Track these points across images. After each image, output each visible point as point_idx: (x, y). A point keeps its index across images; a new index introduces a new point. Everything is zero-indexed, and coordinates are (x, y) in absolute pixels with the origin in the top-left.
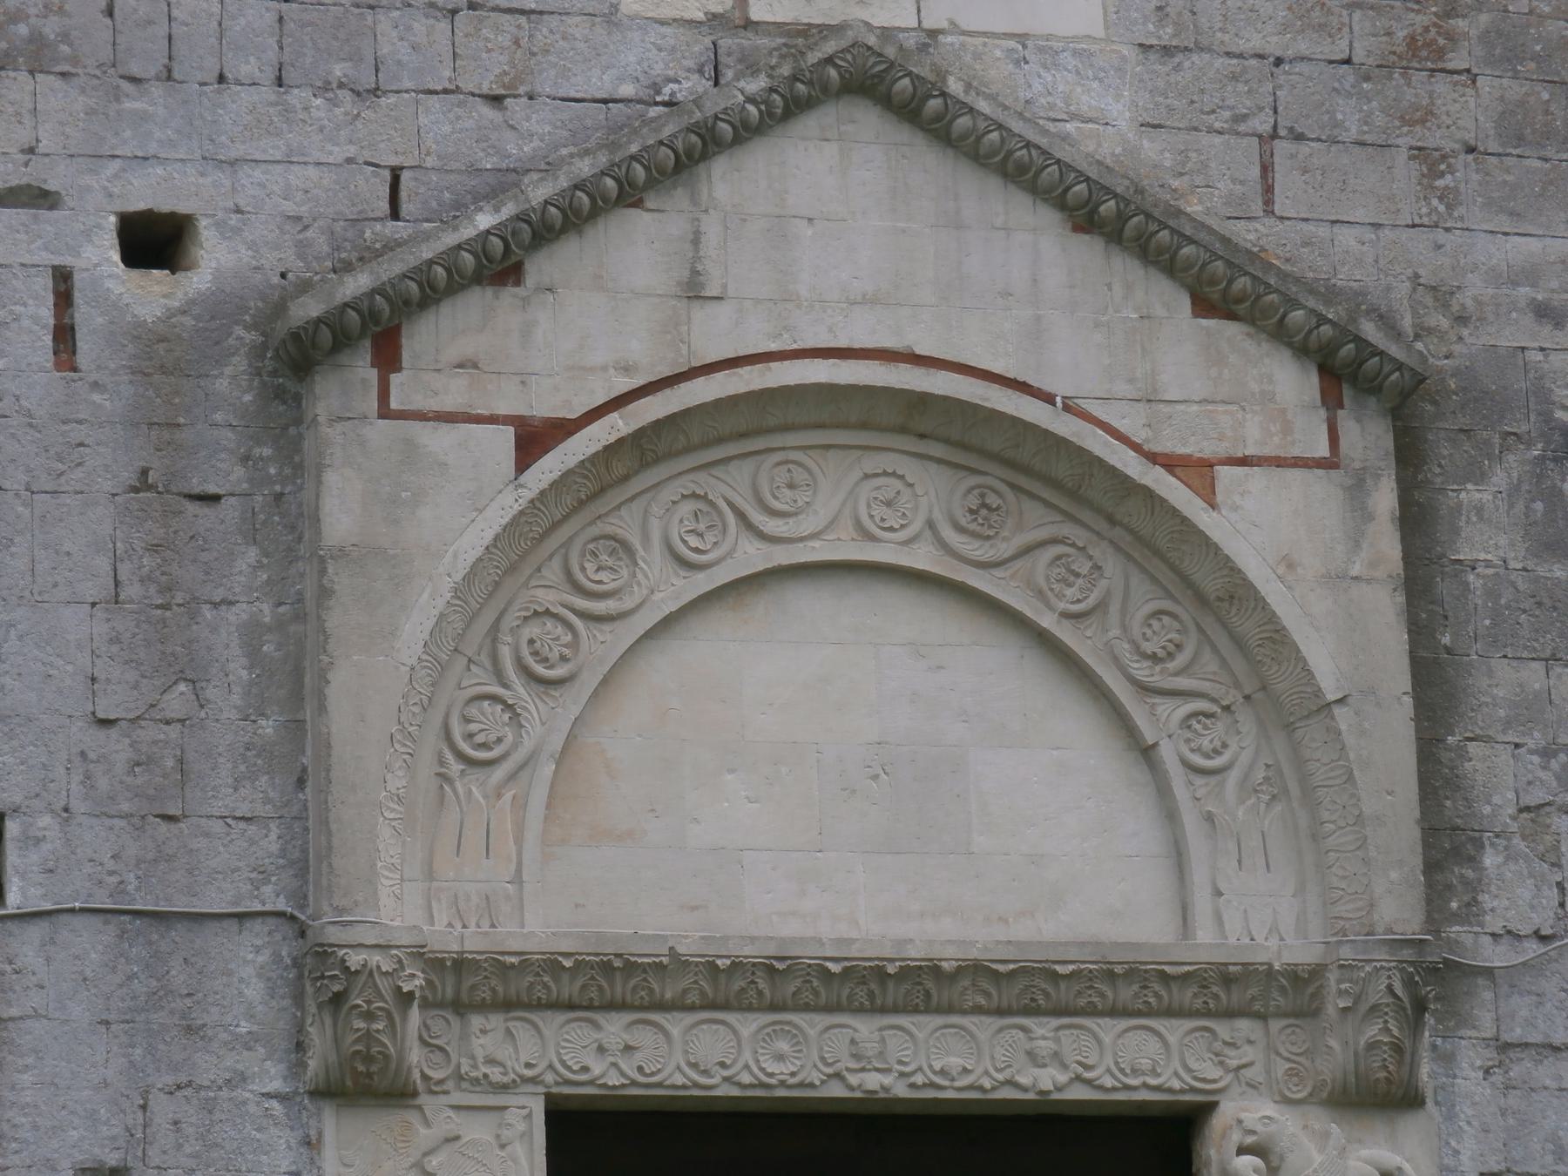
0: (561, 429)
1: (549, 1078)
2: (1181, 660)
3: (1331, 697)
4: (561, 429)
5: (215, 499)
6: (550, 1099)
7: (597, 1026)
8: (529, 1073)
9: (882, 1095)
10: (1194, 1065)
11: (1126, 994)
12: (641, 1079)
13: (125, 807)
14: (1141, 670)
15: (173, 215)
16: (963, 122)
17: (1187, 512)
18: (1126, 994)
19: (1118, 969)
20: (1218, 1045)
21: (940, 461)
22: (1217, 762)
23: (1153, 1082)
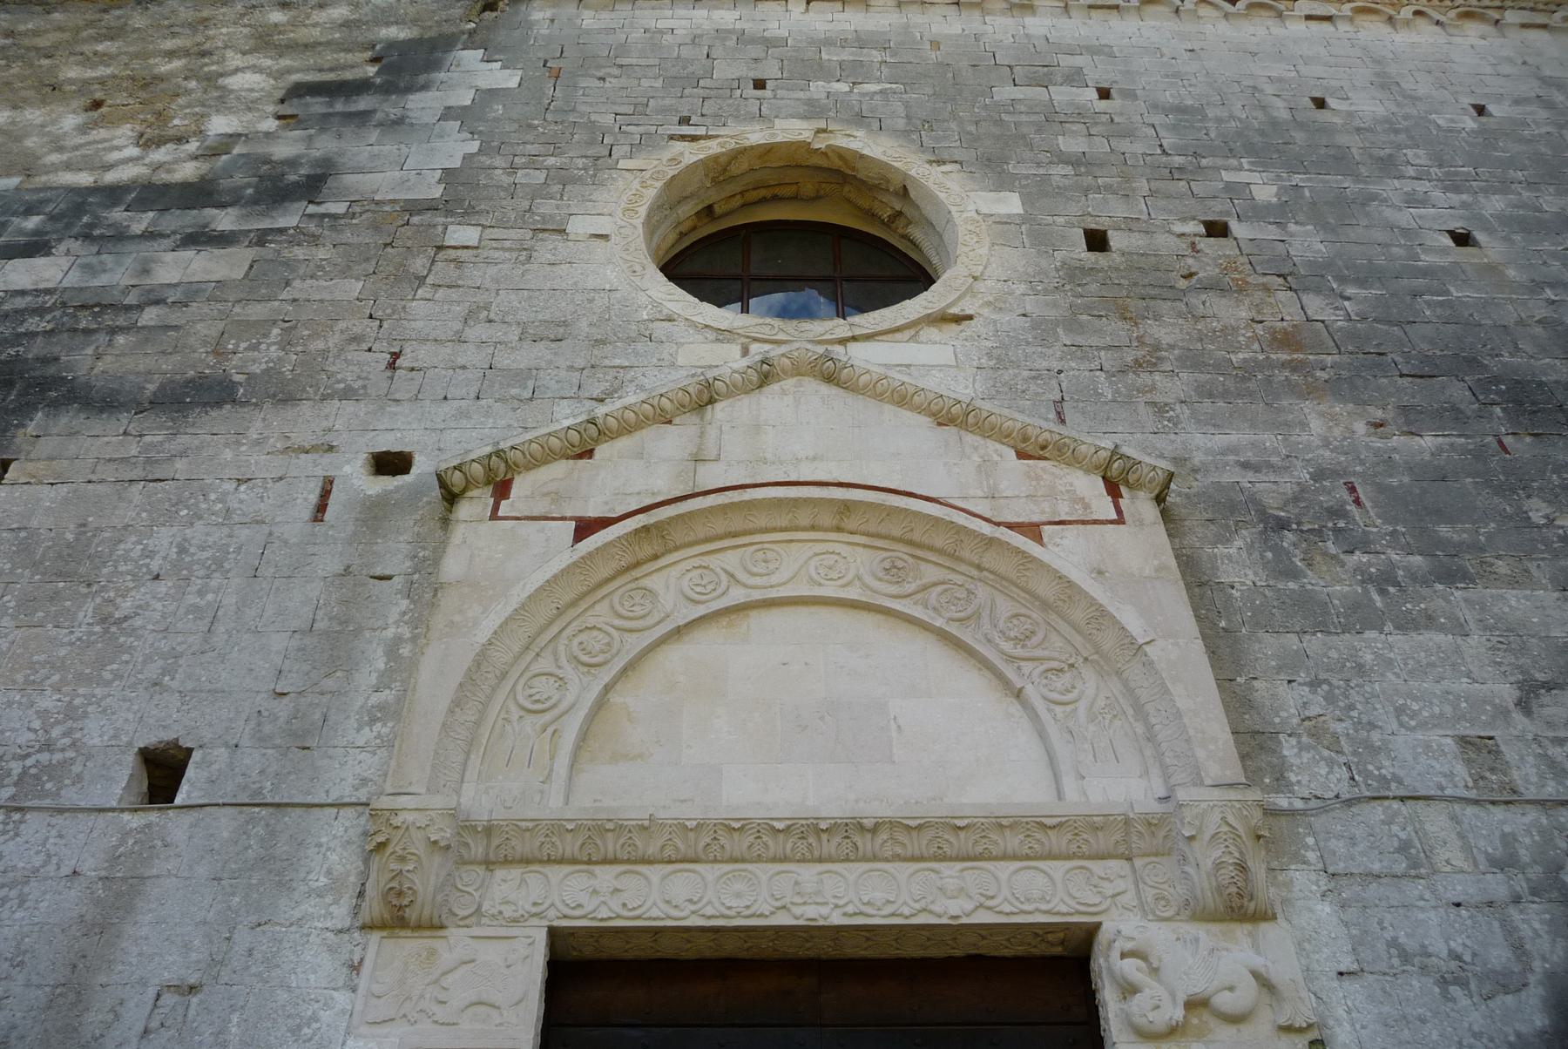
0: (605, 523)
1: (552, 913)
2: (1035, 640)
3: (1141, 641)
4: (605, 523)
5: (389, 578)
6: (553, 933)
7: (593, 874)
8: (534, 910)
9: (821, 923)
10: (1074, 892)
11: (1013, 842)
12: (626, 913)
13: (278, 741)
14: (1007, 647)
15: (400, 453)
16: (864, 379)
17: (1023, 548)
18: (1013, 842)
19: (1005, 822)
20: (1095, 880)
21: (865, 546)
22: (1069, 697)
23: (1044, 907)
